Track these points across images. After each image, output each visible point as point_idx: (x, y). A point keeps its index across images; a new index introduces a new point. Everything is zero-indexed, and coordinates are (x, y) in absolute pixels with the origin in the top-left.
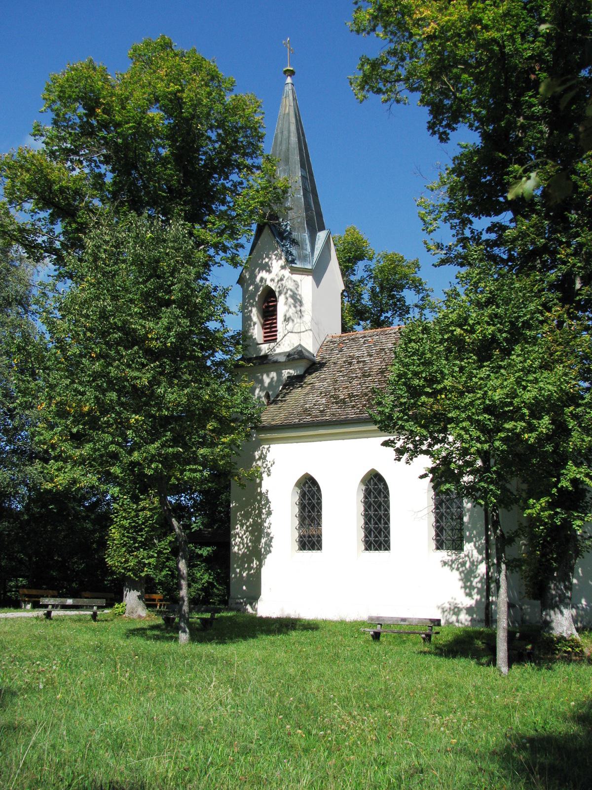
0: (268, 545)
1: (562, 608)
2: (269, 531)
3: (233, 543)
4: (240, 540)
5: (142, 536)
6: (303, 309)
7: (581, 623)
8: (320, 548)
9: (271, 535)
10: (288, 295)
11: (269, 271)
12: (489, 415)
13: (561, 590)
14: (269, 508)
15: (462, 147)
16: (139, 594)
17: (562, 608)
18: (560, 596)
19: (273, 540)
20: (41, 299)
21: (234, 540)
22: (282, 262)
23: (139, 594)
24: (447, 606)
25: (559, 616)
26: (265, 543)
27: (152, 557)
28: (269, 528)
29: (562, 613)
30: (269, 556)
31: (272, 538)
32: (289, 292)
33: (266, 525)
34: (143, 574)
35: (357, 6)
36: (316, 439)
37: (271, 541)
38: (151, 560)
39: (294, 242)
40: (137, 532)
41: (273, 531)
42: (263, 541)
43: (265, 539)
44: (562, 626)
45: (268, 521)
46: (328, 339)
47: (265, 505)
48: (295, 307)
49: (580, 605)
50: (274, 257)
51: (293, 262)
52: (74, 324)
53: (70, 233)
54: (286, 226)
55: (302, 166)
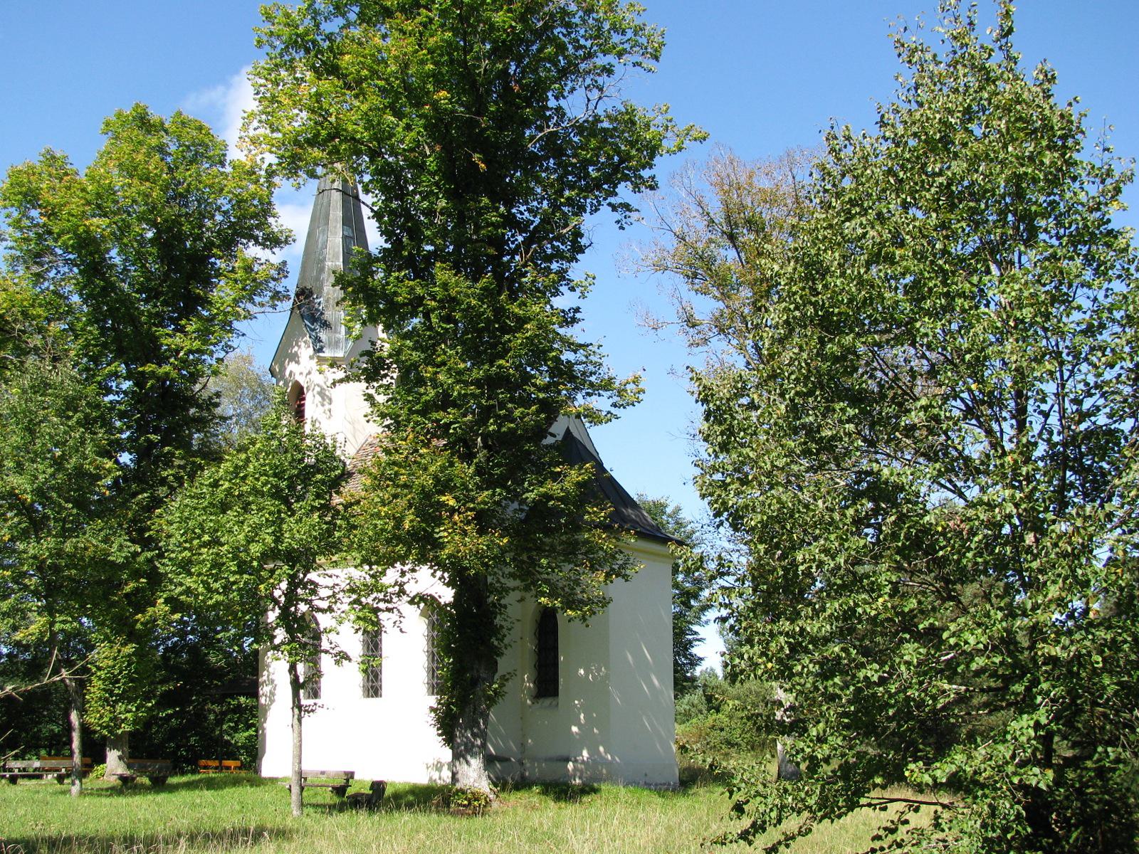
1: (469, 757)
5: (119, 688)
6: (332, 407)
7: (580, 778)
10: (315, 392)
11: (298, 362)
13: (467, 738)
16: (120, 753)
17: (469, 757)
18: (466, 745)
20: (1050, 516)
22: (311, 351)
23: (120, 753)
24: (430, 763)
25: (465, 766)
27: (130, 711)
29: (467, 762)
30: (273, 707)
32: (318, 389)
34: (120, 732)
35: (1074, 103)
38: (129, 715)
39: (326, 325)
40: (113, 684)
44: (468, 777)
46: (370, 440)
48: (323, 405)
49: (579, 758)
50: (303, 344)
51: (321, 350)
54: (319, 304)
55: (346, 221)
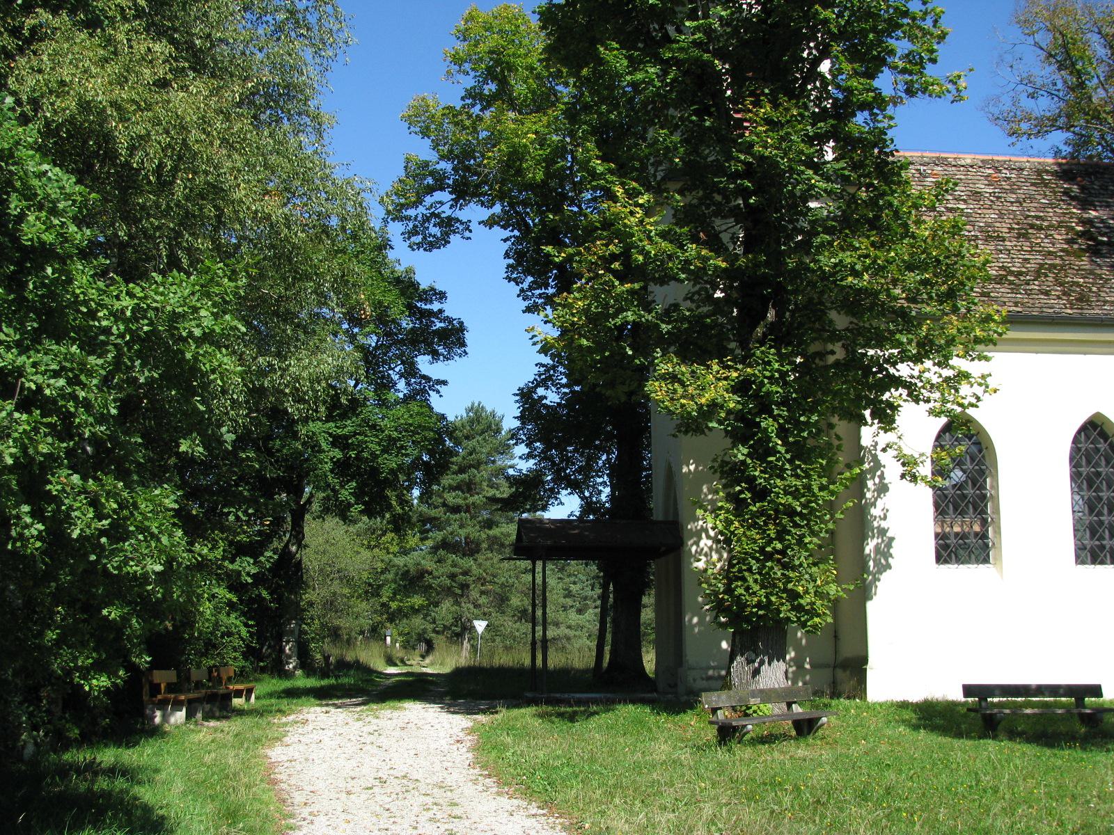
0: (884, 552)
2: (884, 524)
3: (694, 549)
4: (710, 543)
8: (1080, 560)
9: (889, 534)
12: (292, 521)
14: (882, 477)
15: (438, 392)
19: (894, 544)
21: (697, 543)
26: (877, 548)
28: (885, 518)
30: (885, 577)
31: (892, 539)
33: (874, 511)
36: (1044, 348)
37: (889, 545)
41: (893, 526)
42: (870, 547)
43: (875, 541)
45: (880, 503)
47: (873, 471)
52: (127, 81)
53: (131, 668)
